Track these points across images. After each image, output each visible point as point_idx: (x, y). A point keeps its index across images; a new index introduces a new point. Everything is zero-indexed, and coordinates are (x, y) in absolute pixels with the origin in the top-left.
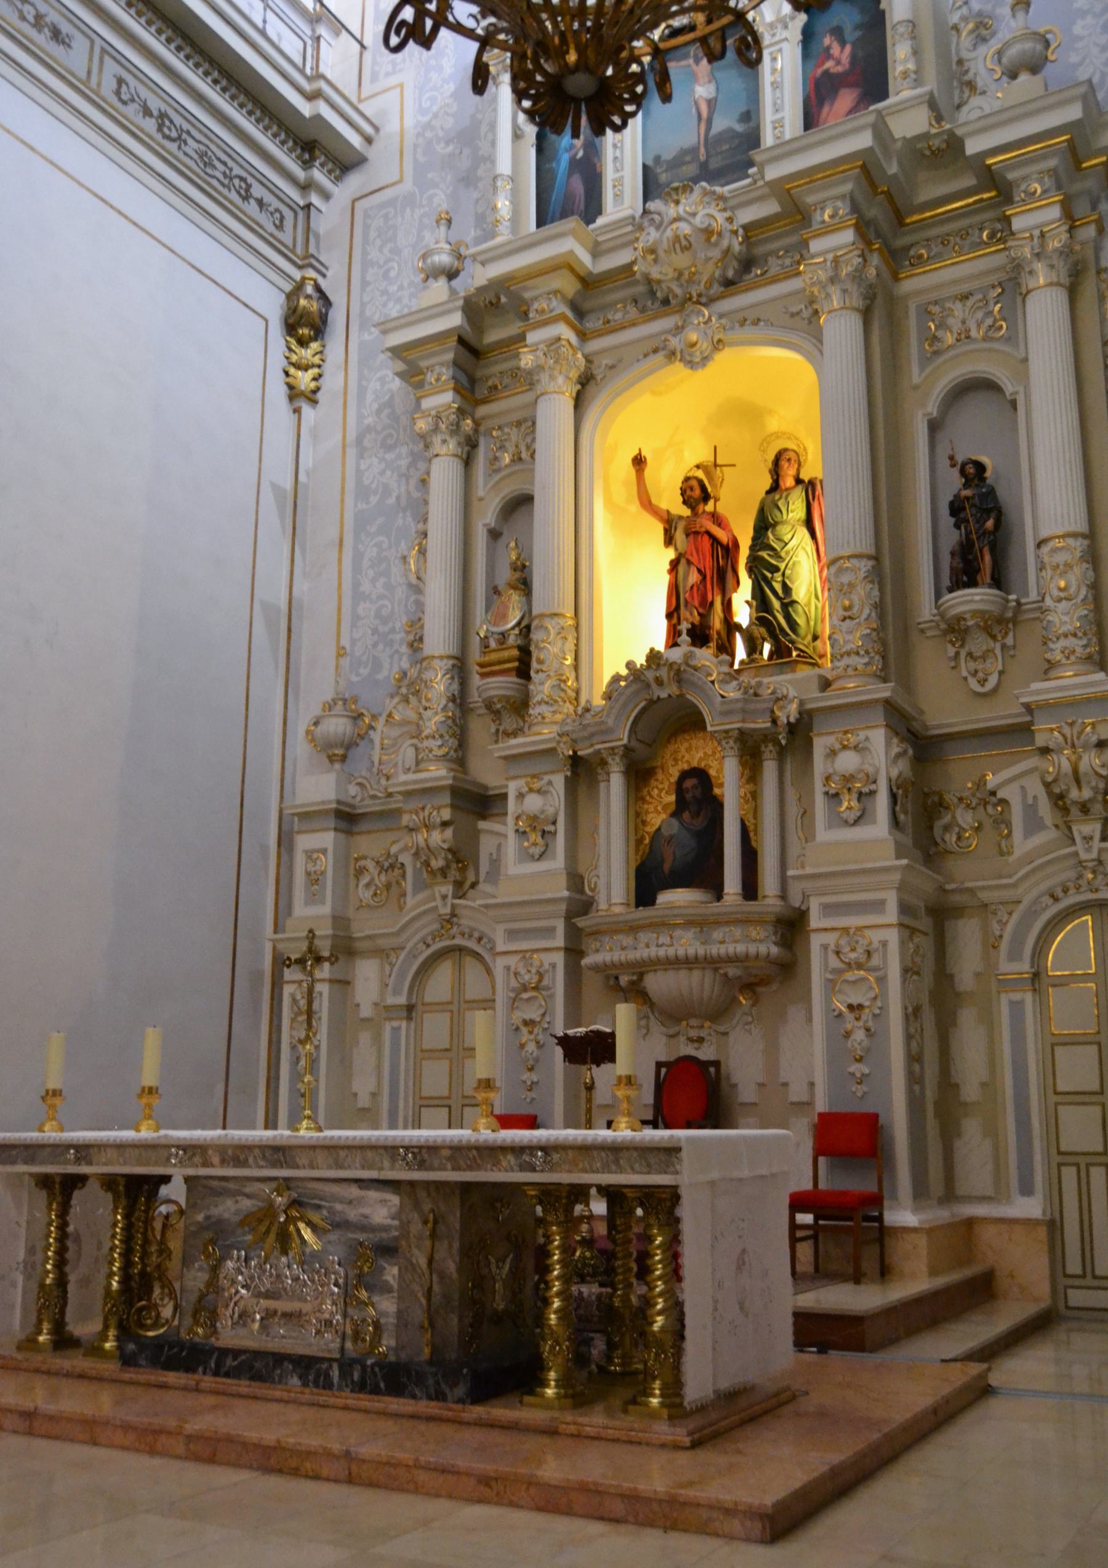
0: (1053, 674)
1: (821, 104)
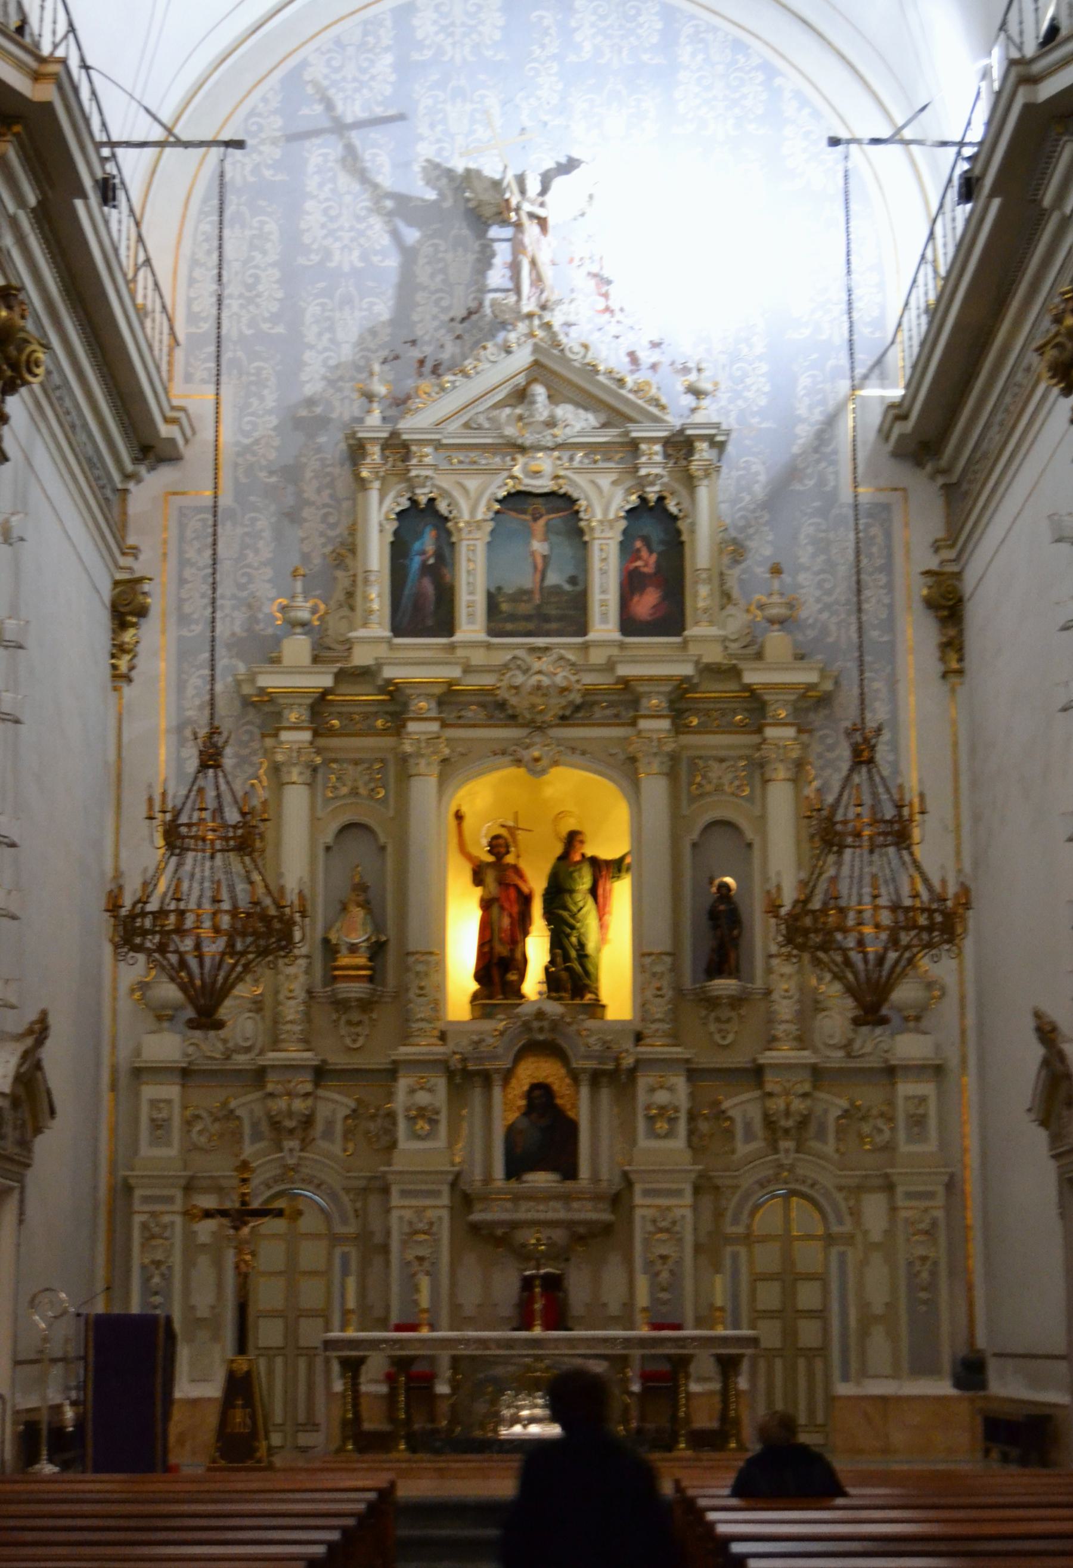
0: (775, 1045)
1: (632, 594)
